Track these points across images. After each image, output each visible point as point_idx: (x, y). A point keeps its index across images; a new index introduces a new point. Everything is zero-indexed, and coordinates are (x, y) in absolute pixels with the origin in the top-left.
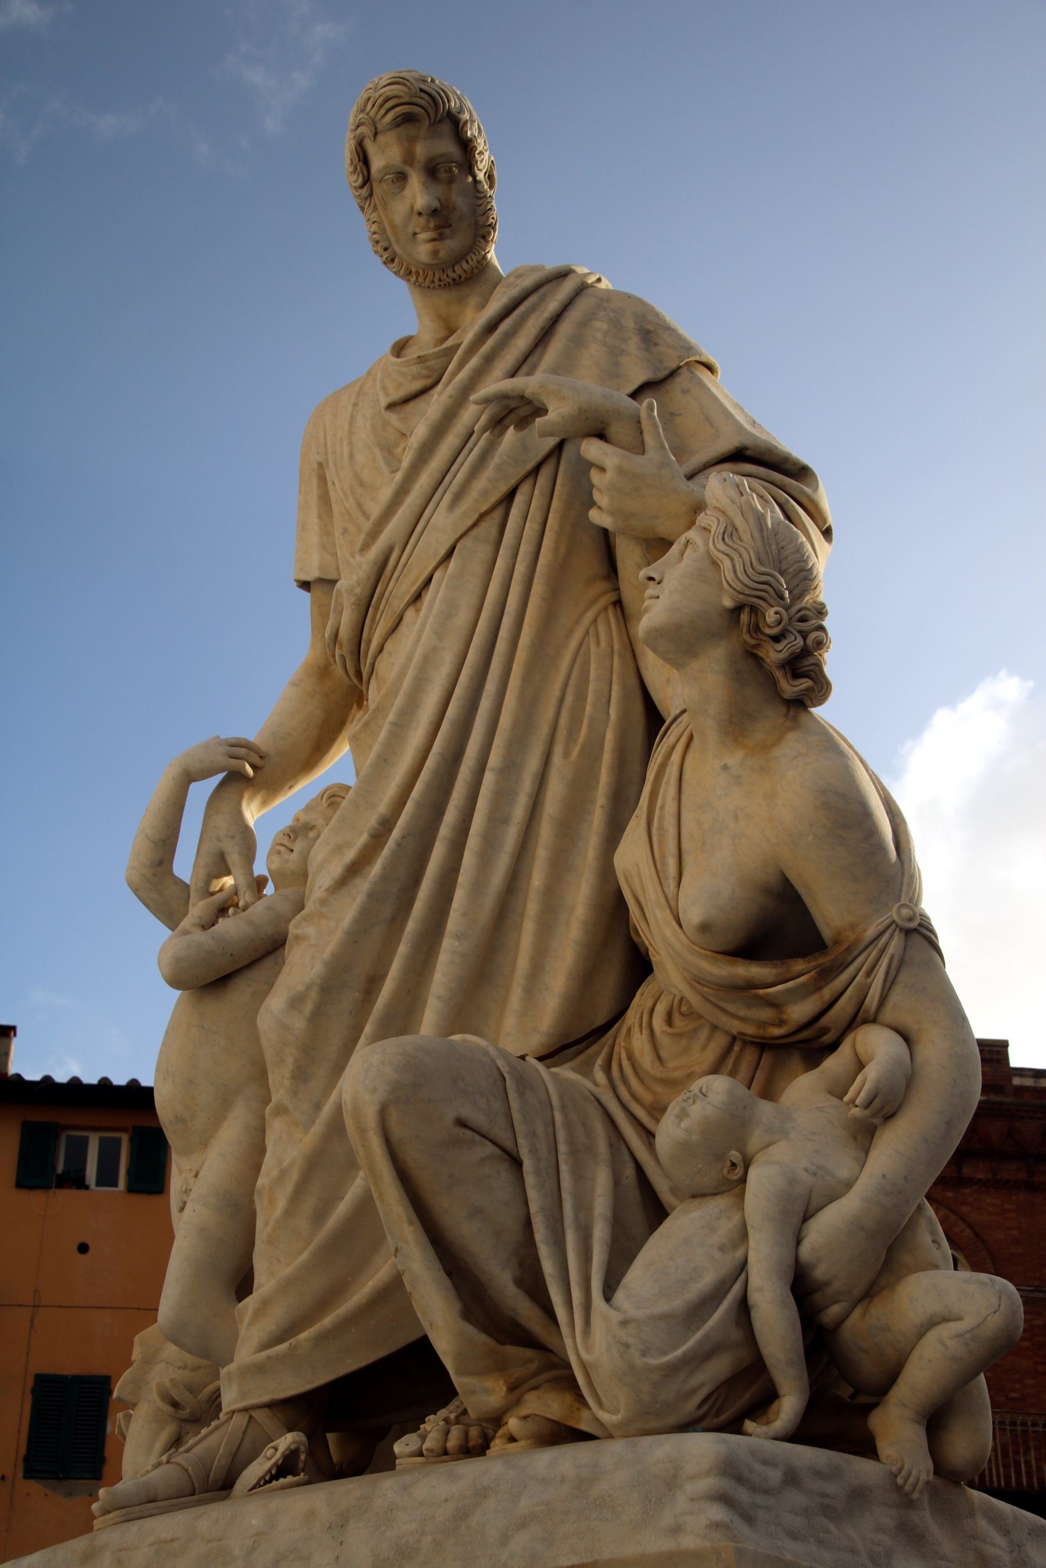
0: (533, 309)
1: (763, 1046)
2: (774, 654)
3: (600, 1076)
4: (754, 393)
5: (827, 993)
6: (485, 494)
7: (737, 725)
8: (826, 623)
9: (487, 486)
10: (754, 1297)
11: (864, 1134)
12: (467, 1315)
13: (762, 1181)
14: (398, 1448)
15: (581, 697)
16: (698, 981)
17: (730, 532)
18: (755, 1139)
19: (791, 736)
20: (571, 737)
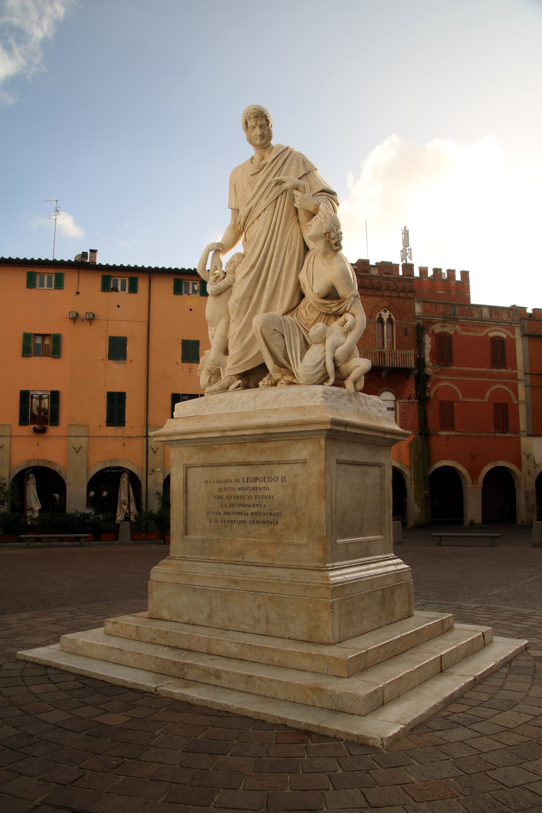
0: (281, 157)
1: (327, 314)
2: (333, 242)
3: (296, 318)
4: (326, 176)
5: (340, 307)
6: (272, 198)
7: (325, 254)
8: (342, 236)
9: (272, 196)
10: (326, 362)
11: (346, 334)
12: (275, 363)
13: (329, 342)
14: (259, 384)
15: (292, 242)
16: (316, 302)
17: (325, 217)
18: (327, 334)
19: (335, 258)
20: (290, 250)
